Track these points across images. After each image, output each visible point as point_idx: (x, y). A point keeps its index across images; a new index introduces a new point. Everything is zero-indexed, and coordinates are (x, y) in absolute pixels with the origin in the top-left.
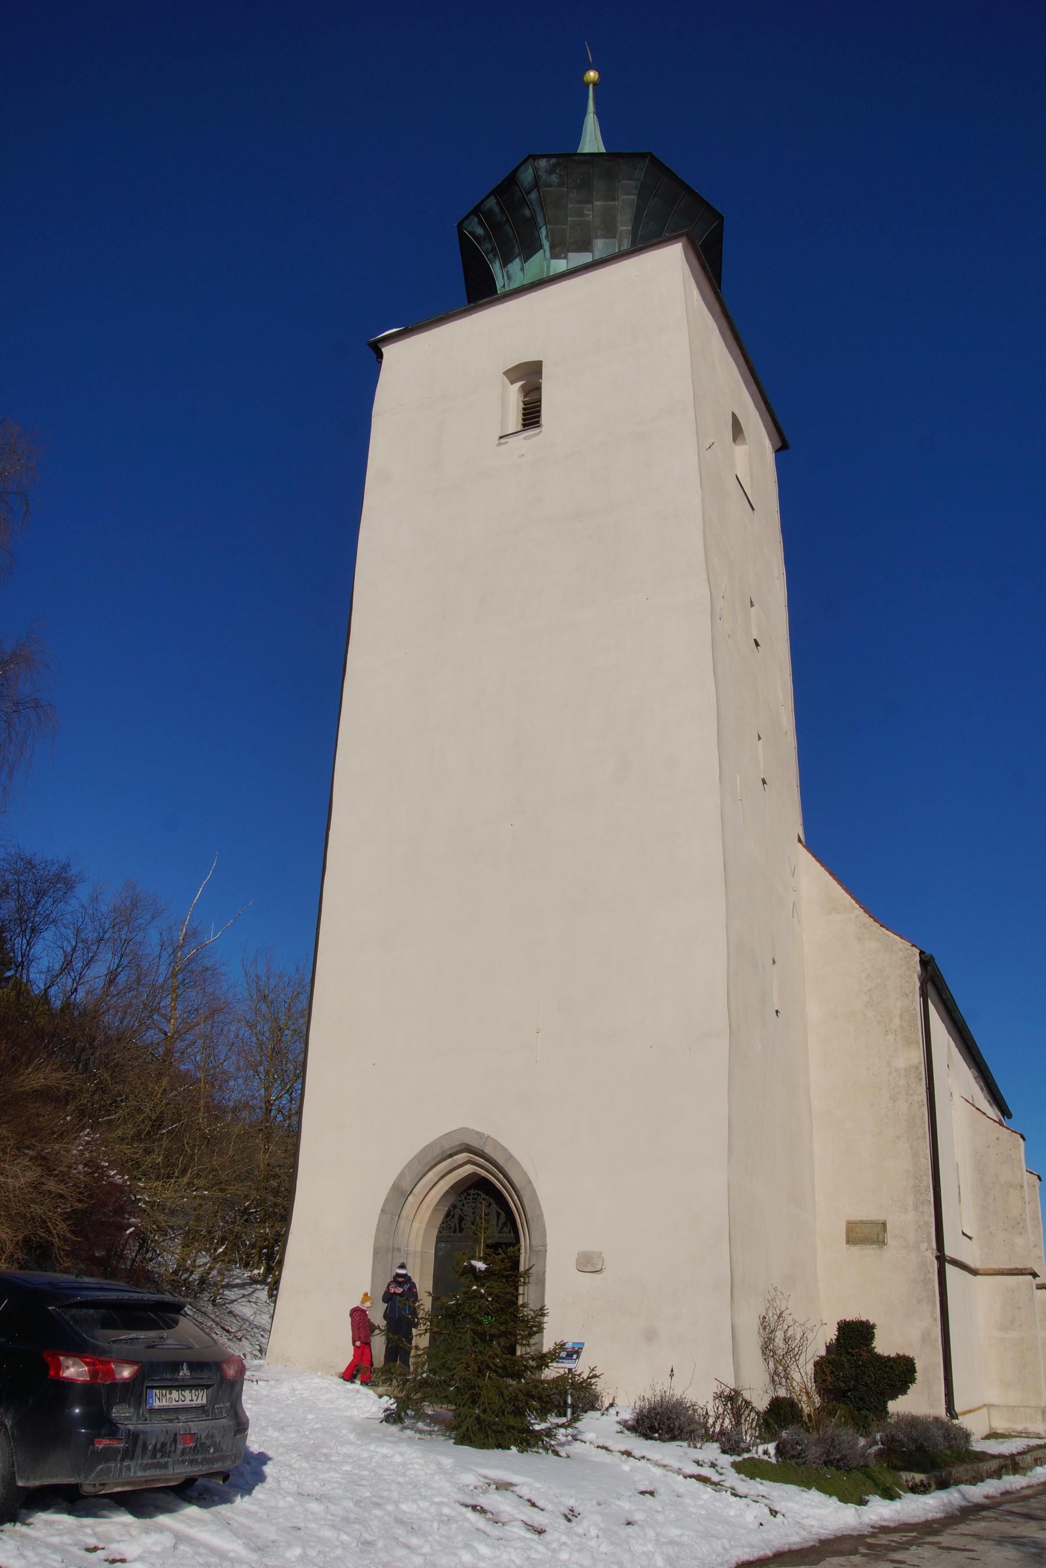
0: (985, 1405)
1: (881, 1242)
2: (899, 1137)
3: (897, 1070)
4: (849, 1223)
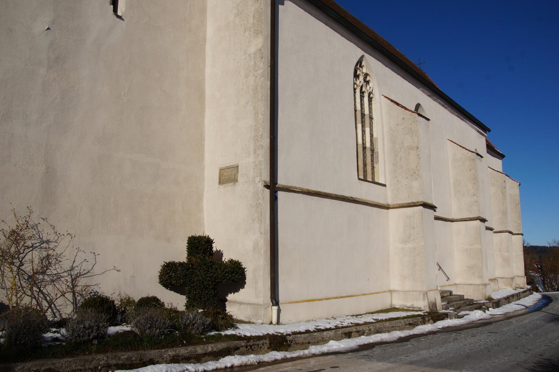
1: (234, 180)
2: (247, 103)
3: (250, 55)
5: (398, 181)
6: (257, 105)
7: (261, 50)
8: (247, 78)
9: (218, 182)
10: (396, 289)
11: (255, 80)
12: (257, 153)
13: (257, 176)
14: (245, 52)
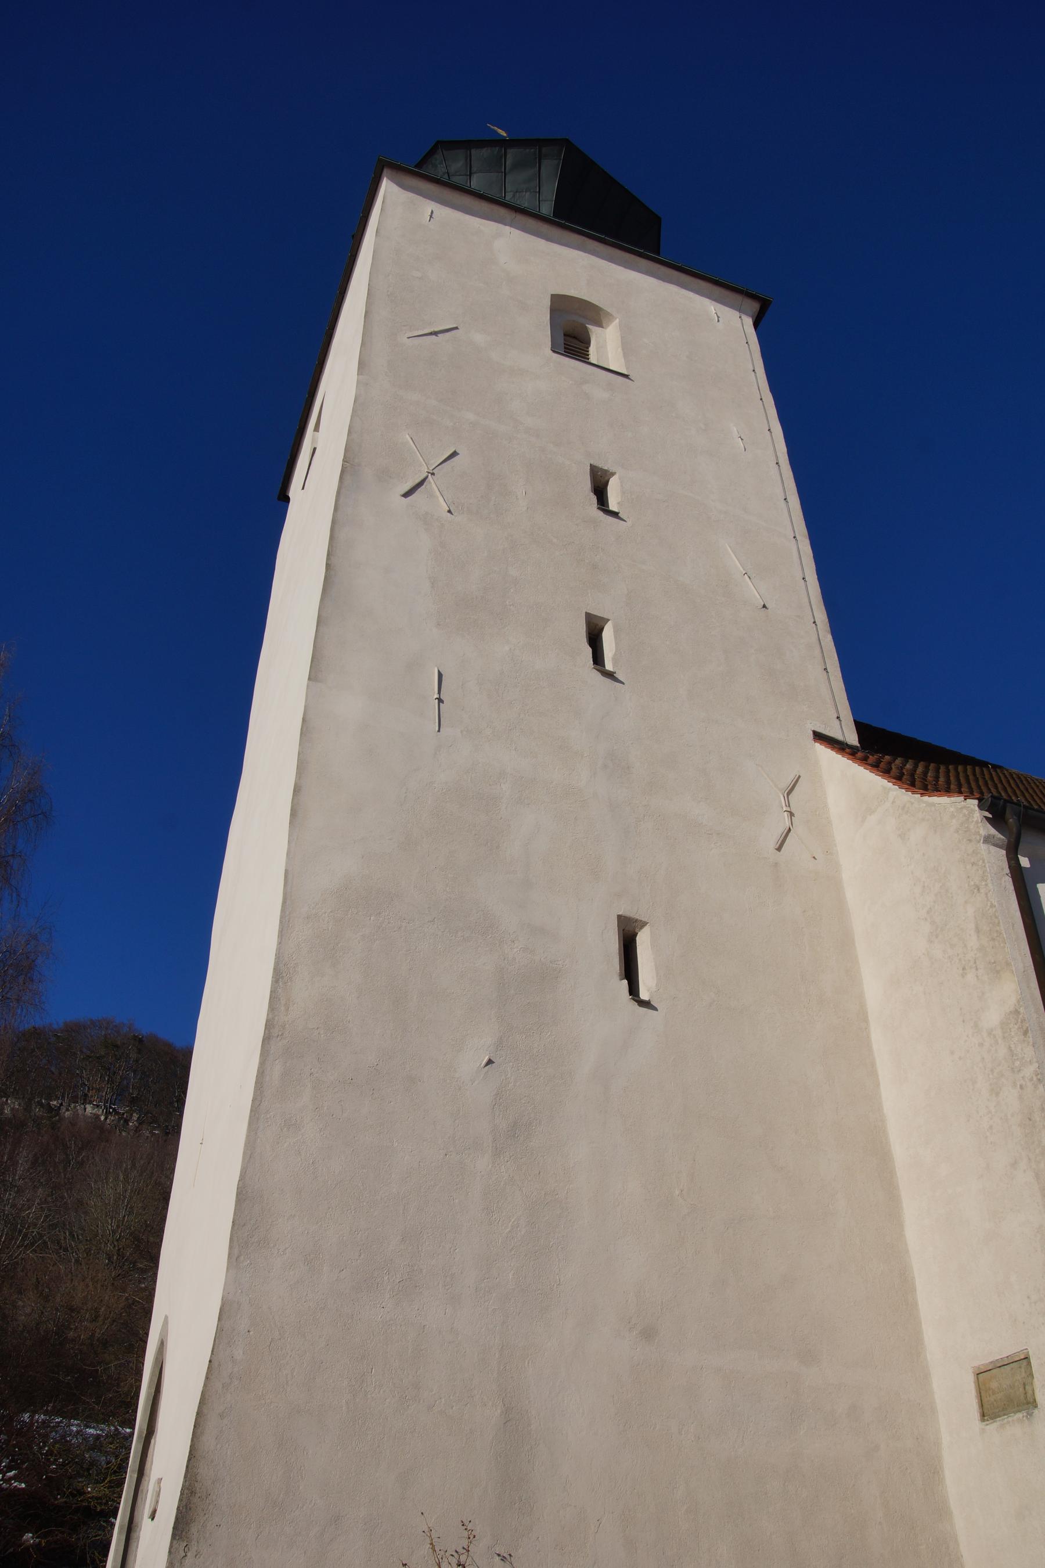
2: (1014, 1165)
3: (990, 1033)
4: (979, 1374)
7: (1017, 1012)
8: (997, 1094)
11: (1020, 1098)
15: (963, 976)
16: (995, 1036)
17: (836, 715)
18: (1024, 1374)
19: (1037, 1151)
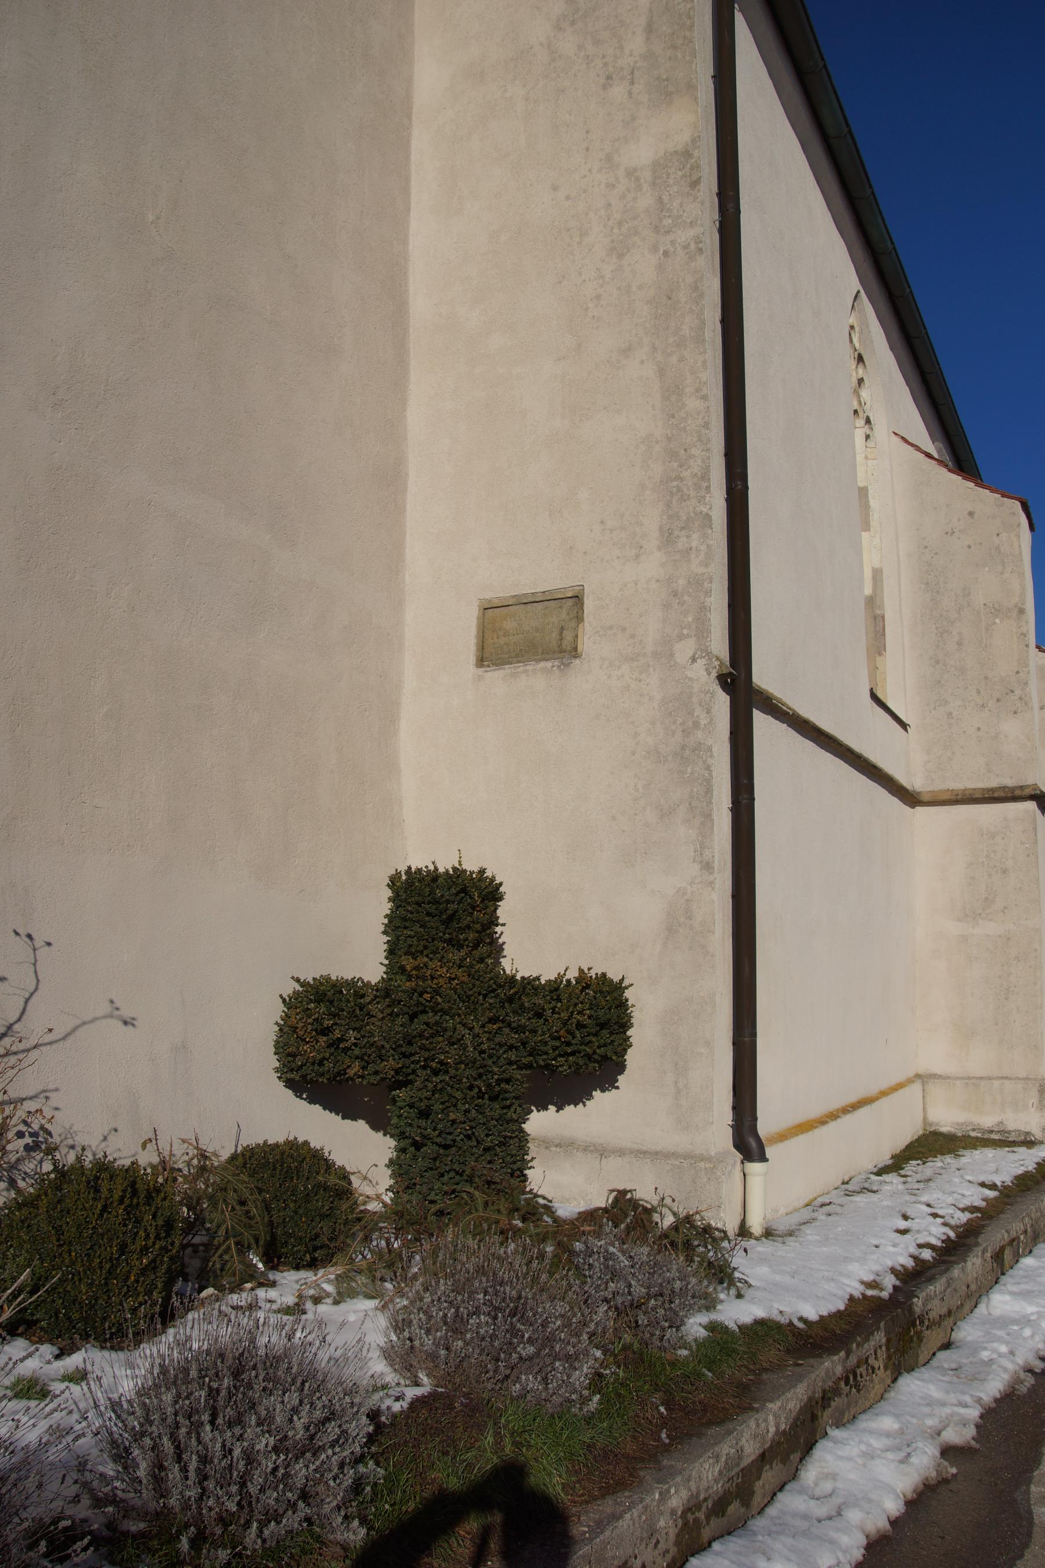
0: (918, 1076)
1: (564, 651)
2: (627, 351)
3: (631, 173)
4: (486, 608)
5: (950, 715)
6: (674, 359)
7: (687, 154)
8: (621, 256)
9: (472, 659)
10: (938, 1071)
11: (660, 268)
12: (682, 543)
13: (681, 637)
14: (609, 158)
15: (604, 87)
16: (638, 179)
17: (120, 1024)
18: (564, 616)
19: (671, 340)
